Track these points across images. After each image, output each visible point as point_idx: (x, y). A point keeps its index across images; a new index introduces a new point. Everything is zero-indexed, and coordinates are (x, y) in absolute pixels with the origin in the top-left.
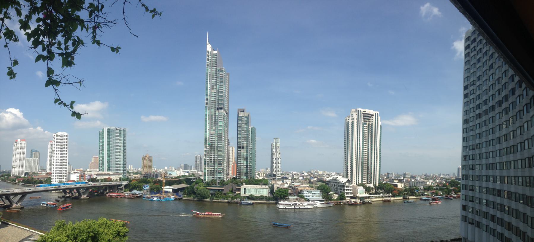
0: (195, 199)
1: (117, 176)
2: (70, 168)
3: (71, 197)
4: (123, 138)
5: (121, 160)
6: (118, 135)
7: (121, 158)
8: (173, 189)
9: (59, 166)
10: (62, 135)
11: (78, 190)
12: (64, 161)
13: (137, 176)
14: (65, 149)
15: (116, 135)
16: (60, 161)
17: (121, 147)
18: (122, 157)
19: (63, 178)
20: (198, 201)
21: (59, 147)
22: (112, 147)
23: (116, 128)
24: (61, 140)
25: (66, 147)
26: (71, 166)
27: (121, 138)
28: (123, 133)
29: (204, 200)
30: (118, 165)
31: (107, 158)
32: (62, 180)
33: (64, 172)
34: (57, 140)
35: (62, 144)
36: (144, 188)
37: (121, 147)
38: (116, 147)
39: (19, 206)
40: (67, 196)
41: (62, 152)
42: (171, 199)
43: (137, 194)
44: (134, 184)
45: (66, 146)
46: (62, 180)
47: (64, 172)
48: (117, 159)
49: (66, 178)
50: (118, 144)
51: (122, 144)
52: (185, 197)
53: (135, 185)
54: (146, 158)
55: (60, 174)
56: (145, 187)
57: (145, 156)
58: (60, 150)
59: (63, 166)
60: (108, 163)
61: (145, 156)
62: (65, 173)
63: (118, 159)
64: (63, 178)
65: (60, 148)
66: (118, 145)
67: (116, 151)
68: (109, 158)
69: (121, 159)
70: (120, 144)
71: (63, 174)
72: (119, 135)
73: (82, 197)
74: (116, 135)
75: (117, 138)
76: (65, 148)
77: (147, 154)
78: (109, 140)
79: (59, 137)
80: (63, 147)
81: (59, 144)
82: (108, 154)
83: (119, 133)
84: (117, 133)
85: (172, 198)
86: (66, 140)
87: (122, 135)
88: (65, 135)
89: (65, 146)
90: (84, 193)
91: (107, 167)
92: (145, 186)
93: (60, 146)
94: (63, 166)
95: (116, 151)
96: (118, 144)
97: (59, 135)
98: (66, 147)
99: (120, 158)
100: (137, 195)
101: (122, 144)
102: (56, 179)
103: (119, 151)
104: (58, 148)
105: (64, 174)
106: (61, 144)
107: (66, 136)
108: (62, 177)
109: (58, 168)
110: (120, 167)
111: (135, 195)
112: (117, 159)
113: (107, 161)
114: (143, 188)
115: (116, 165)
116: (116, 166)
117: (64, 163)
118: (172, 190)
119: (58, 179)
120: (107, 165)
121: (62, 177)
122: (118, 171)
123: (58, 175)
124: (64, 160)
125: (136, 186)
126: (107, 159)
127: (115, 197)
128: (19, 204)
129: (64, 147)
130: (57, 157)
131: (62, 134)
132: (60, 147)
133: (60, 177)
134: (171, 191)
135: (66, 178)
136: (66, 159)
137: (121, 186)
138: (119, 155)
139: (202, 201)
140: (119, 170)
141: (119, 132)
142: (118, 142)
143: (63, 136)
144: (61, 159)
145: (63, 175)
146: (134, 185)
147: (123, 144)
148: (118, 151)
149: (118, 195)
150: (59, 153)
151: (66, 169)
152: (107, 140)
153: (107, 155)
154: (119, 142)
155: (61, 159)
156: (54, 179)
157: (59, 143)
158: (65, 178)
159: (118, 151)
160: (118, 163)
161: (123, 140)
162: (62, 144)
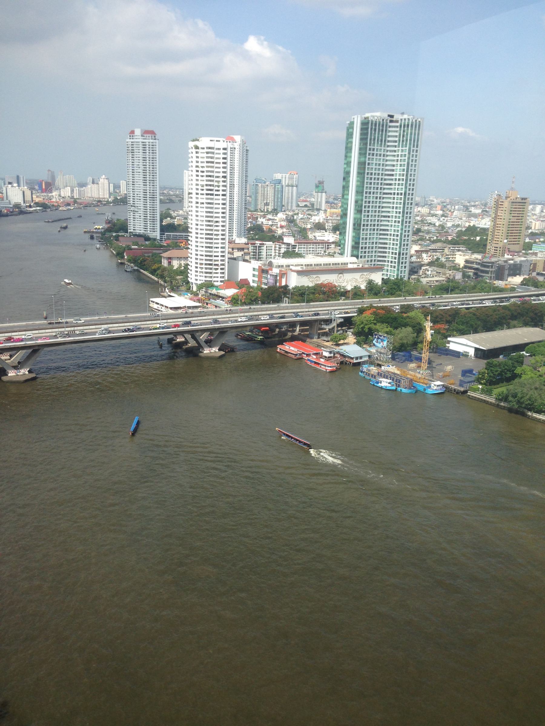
0: (502, 404)
1: (365, 274)
2: (319, 200)
3: (184, 347)
4: (409, 153)
5: (395, 222)
6: (396, 142)
7: (398, 215)
8: (477, 350)
9: (204, 240)
10: (210, 148)
11: (193, 334)
12: (217, 226)
13: (283, 352)
14: (221, 193)
15: (390, 139)
16: (206, 225)
17: (399, 180)
18: (400, 213)
19: (214, 271)
20: (510, 410)
21: (202, 186)
22: (373, 181)
23: (392, 116)
24: (207, 162)
25: (223, 186)
26: (324, 194)
27: (402, 151)
28: (411, 134)
29: (530, 413)
30: (387, 235)
31: (355, 214)
32: (211, 277)
33: (218, 256)
34: (197, 162)
35: (210, 176)
36: (376, 343)
37: (399, 180)
38: (385, 180)
39: (24, 374)
40: (178, 340)
41: (212, 199)
42: (429, 391)
43: (352, 358)
44: (362, 323)
45: (221, 184)
46: (211, 277)
47: (218, 256)
48: (385, 217)
49: (223, 273)
50: (393, 170)
51: (404, 170)
52: (475, 390)
53: (363, 328)
54: (506, 204)
55: (206, 260)
56: (379, 340)
57: (504, 195)
58: (207, 194)
59: (215, 239)
60: (354, 229)
61: (504, 195)
62: (220, 258)
63: (389, 217)
64: (214, 271)
65: (205, 188)
66: (392, 175)
67: (384, 194)
68: (358, 216)
69: (397, 220)
70: (398, 171)
71: (215, 261)
72: (397, 139)
73: (205, 352)
74: (390, 139)
75: (391, 151)
76: (221, 188)
77: (512, 189)
78: (362, 159)
79: (202, 154)
80: (213, 185)
81: (202, 176)
82: (356, 202)
83: (400, 135)
84: (393, 133)
85: (435, 388)
86: (224, 163)
87: (407, 140)
88: (219, 149)
89: (218, 182)
90: (209, 343)
91: (353, 241)
92: (378, 338)
93: (205, 183)
94: (215, 239)
95: (384, 194)
96: (393, 170)
97: (203, 148)
98: (223, 186)
99: (394, 215)
100: (351, 361)
101: (404, 170)
102: (198, 274)
103: (394, 194)
104: (200, 187)
105: (218, 260)
106: (207, 176)
107: (222, 151)
108: (211, 269)
109: (202, 245)
110: (392, 242)
111: (347, 359)
112: (385, 217)
113: (354, 225)
114: (374, 342)
115: (380, 234)
116: (380, 238)
117: (218, 231)
118: (473, 350)
119: (201, 274)
120: (353, 237)
121: (211, 269)
122: (385, 252)
123: (201, 264)
124: (217, 222)
125: (367, 330)
126: (355, 219)
127: (293, 356)
128: (24, 371)
129: (216, 184)
130: (199, 214)
131: (211, 145)
132: (207, 185)
133: (206, 268)
134: (472, 352)
135: (223, 273)
136: (223, 222)
137: (331, 322)
138: (391, 205)
139: (524, 415)
140: (387, 246)
141: (400, 130)
142: (394, 166)
143: (213, 153)
144: (209, 221)
145: (215, 265)
146: (362, 326)
147: (407, 171)
148: (391, 194)
149: (304, 353)
150: (203, 203)
151: (222, 248)
152: (359, 158)
153: (356, 206)
154: (395, 163)
155: (209, 221)
156: (193, 273)
157: (203, 172)
158: (219, 271)
159: (391, 194)
160: (387, 230)
161: (409, 158)
162: (210, 176)
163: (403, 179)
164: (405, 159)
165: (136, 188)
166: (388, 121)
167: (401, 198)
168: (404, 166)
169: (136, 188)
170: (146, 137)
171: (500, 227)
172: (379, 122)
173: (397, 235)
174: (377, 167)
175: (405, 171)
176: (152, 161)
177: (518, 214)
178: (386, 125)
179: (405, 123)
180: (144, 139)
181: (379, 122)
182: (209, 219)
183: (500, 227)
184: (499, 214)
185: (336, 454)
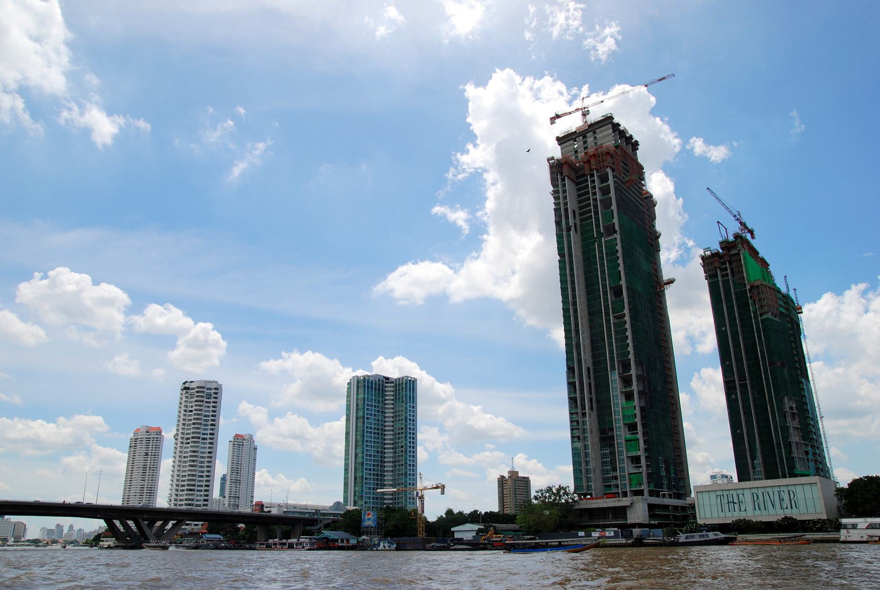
17: (399, 434)
37: (399, 434)
163: (402, 433)
164: (403, 428)
165: (131, 499)
166: (384, 382)
167: (402, 423)
168: (402, 420)
169: (131, 499)
170: (152, 433)
171: (507, 505)
172: (376, 382)
173: (402, 447)
174: (376, 431)
175: (404, 420)
176: (154, 460)
177: (522, 492)
178: (382, 385)
179: (399, 383)
180: (148, 435)
181: (376, 382)
182: (191, 487)
183: (507, 505)
184: (504, 493)
185: (100, 515)
